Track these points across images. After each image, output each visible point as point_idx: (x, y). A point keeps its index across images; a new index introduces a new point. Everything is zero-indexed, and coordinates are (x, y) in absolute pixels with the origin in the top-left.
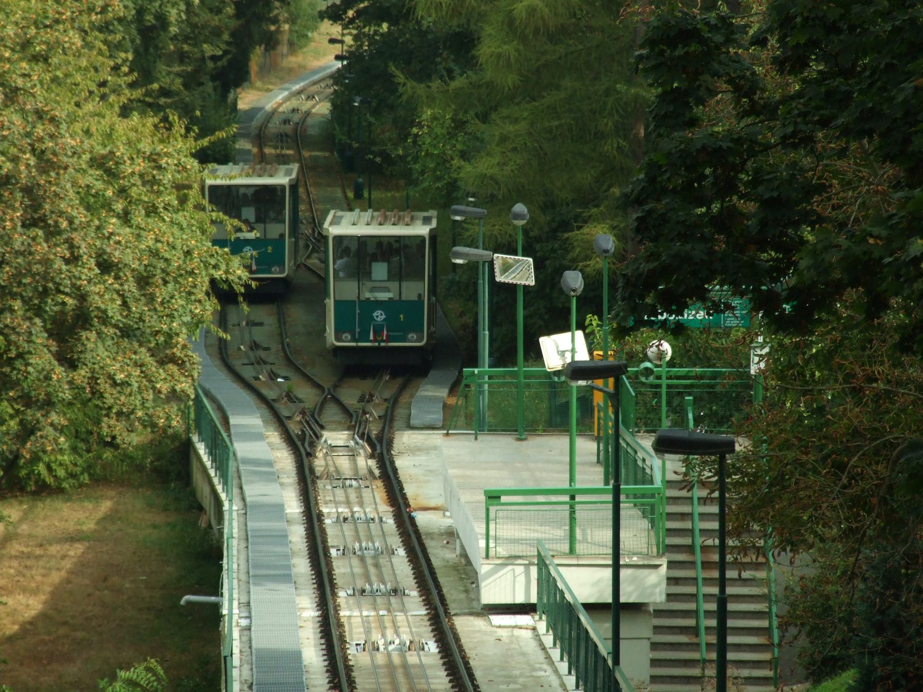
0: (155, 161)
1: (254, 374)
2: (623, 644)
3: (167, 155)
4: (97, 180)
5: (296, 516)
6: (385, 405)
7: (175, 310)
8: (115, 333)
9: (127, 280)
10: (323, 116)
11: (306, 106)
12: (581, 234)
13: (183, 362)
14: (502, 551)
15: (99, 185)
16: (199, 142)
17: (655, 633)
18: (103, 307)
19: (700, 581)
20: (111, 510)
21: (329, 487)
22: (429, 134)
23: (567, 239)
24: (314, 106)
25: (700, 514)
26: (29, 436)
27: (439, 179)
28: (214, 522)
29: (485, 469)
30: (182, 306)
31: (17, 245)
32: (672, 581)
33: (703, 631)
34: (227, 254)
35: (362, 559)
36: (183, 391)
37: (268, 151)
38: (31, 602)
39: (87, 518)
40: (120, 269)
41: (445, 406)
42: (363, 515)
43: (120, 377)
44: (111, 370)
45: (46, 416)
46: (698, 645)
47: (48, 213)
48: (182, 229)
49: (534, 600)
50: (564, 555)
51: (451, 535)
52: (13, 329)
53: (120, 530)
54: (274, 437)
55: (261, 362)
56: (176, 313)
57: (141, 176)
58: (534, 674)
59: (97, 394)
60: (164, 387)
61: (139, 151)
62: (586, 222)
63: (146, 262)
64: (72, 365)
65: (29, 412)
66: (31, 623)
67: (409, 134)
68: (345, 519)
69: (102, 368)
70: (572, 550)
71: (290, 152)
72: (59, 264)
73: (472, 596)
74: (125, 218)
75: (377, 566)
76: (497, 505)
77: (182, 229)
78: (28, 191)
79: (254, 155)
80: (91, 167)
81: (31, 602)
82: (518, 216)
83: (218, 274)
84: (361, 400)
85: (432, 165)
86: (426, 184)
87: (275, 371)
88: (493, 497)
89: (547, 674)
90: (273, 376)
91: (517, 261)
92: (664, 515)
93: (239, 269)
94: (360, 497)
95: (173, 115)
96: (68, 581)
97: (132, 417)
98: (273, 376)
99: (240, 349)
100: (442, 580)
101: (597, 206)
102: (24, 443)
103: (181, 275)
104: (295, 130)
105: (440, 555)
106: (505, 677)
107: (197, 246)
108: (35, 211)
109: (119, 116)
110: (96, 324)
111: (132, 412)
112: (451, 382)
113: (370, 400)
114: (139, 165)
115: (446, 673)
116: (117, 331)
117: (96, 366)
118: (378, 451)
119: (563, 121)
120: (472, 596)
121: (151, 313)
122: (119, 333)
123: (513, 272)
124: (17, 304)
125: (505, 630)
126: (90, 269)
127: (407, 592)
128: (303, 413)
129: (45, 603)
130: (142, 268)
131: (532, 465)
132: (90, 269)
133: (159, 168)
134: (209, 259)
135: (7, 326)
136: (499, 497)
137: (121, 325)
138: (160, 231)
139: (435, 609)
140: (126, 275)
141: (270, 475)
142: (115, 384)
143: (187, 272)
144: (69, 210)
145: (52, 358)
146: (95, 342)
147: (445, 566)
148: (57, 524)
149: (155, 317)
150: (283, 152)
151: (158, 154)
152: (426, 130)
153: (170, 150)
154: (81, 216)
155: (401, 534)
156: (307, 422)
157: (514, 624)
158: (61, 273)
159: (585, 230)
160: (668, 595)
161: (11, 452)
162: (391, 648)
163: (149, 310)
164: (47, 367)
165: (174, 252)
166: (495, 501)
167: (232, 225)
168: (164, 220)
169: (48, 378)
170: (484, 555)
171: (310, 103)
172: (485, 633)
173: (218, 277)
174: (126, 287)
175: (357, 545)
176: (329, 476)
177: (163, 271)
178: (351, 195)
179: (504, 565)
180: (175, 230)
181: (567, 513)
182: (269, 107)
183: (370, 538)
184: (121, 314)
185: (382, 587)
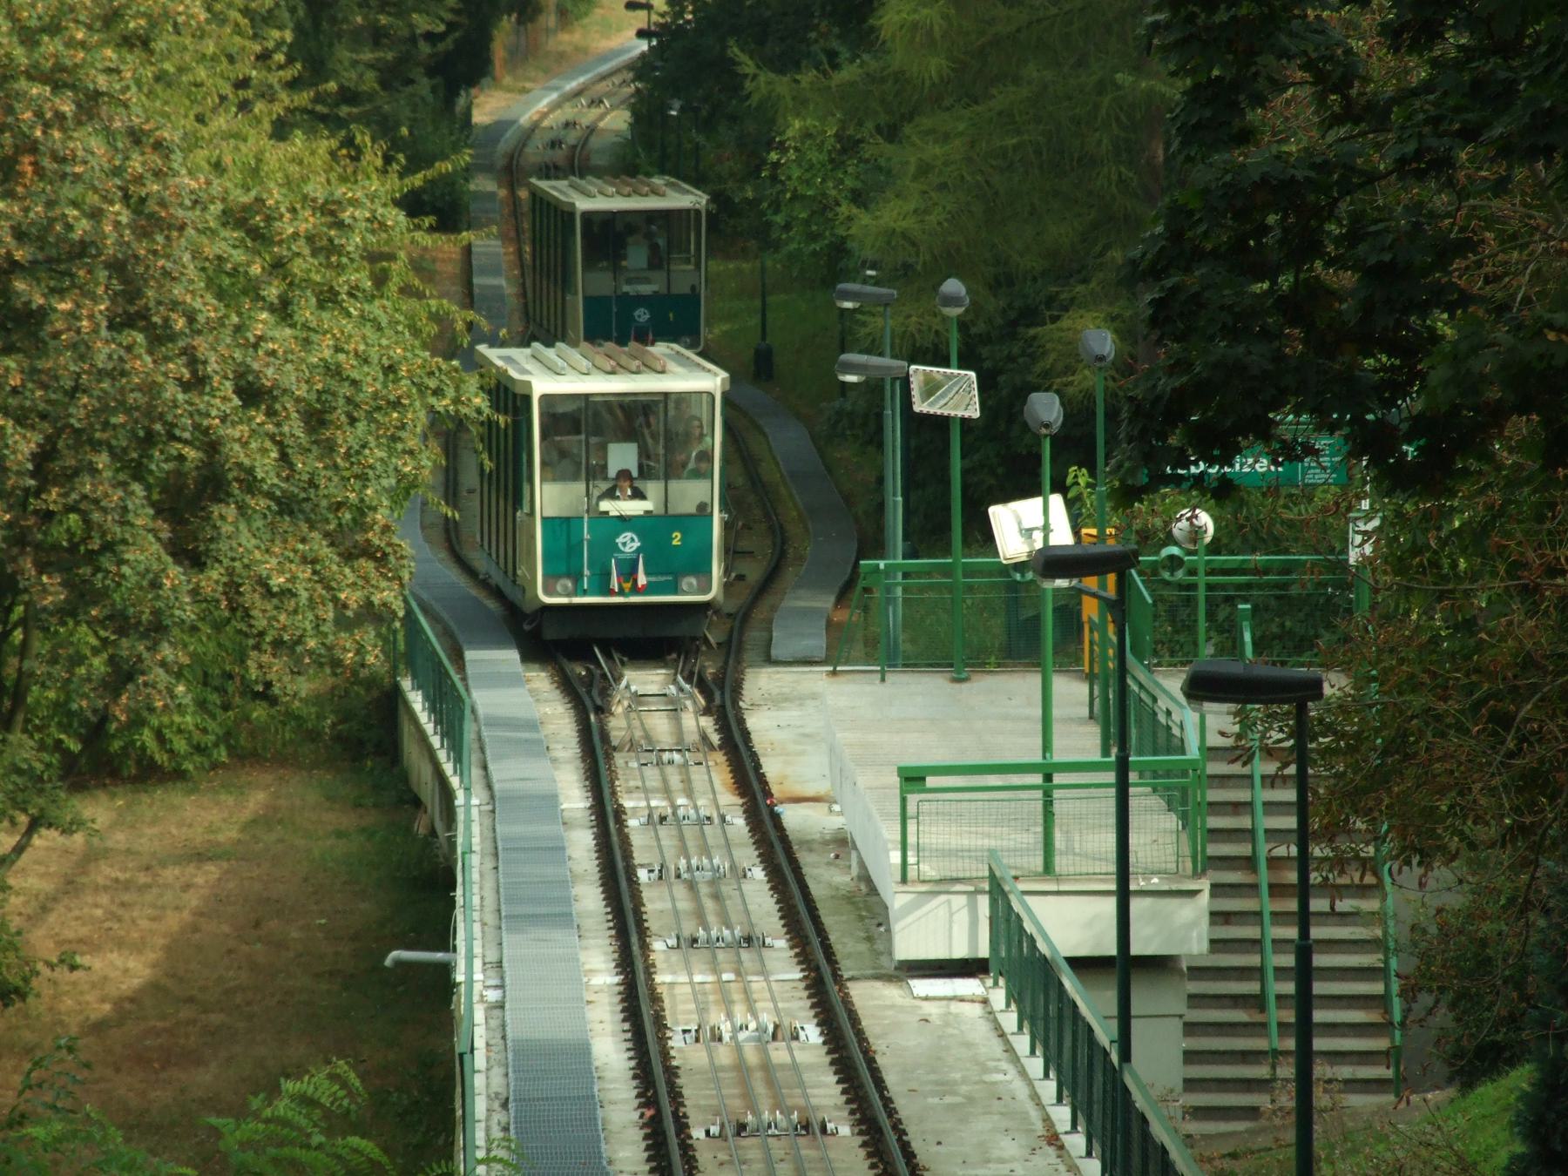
0: (332, 213)
2: (1136, 1026)
3: (354, 203)
4: (235, 247)
5: (579, 815)
7: (371, 467)
8: (269, 507)
9: (287, 417)
10: (618, 133)
13: (385, 555)
14: (929, 870)
16: (407, 181)
18: (247, 462)
19: (1267, 918)
22: (798, 162)
23: (1034, 338)
24: (602, 117)
27: (813, 237)
30: (382, 460)
31: (100, 360)
34: (456, 370)
35: (692, 886)
39: (224, 820)
40: (275, 399)
43: (278, 581)
44: (263, 570)
45: (153, 648)
46: (1264, 1025)
48: (379, 328)
49: (984, 951)
50: (1033, 876)
51: (842, 843)
57: (310, 239)
62: (1066, 309)
63: (319, 386)
65: (125, 642)
67: (764, 162)
69: (247, 567)
72: (171, 391)
73: (880, 946)
74: (283, 310)
75: (717, 897)
77: (379, 328)
78: (118, 267)
80: (224, 225)
82: (951, 301)
83: (441, 404)
85: (803, 215)
86: (793, 246)
88: (913, 779)
89: (1008, 1077)
91: (949, 377)
93: (476, 395)
95: (363, 133)
97: (299, 649)
100: (828, 920)
101: (1085, 281)
103: (379, 408)
105: (824, 878)
107: (405, 358)
108: (131, 301)
110: (236, 492)
111: (300, 641)
112: (837, 590)
114: (306, 220)
115: (835, 1078)
118: (718, 701)
121: (329, 473)
122: (275, 508)
123: (943, 396)
124: (102, 460)
126: (225, 399)
127: (768, 941)
130: (314, 396)
133: (340, 225)
135: (85, 497)
137: (278, 493)
139: (817, 969)
140: (285, 409)
142: (269, 593)
143: (388, 402)
144: (188, 299)
145: (162, 551)
148: (174, 831)
149: (336, 479)
152: (792, 155)
153: (359, 194)
154: (208, 308)
155: (759, 843)
157: (950, 993)
158: (176, 407)
159: (1065, 323)
161: (95, 711)
164: (155, 567)
165: (366, 369)
166: (916, 786)
168: (349, 315)
169: (155, 585)
171: (595, 112)
172: (902, 1009)
173: (441, 409)
174: (286, 429)
177: (349, 400)
180: (368, 331)
181: (1039, 805)
182: (525, 119)
183: (705, 850)
184: (278, 476)
185: (726, 933)
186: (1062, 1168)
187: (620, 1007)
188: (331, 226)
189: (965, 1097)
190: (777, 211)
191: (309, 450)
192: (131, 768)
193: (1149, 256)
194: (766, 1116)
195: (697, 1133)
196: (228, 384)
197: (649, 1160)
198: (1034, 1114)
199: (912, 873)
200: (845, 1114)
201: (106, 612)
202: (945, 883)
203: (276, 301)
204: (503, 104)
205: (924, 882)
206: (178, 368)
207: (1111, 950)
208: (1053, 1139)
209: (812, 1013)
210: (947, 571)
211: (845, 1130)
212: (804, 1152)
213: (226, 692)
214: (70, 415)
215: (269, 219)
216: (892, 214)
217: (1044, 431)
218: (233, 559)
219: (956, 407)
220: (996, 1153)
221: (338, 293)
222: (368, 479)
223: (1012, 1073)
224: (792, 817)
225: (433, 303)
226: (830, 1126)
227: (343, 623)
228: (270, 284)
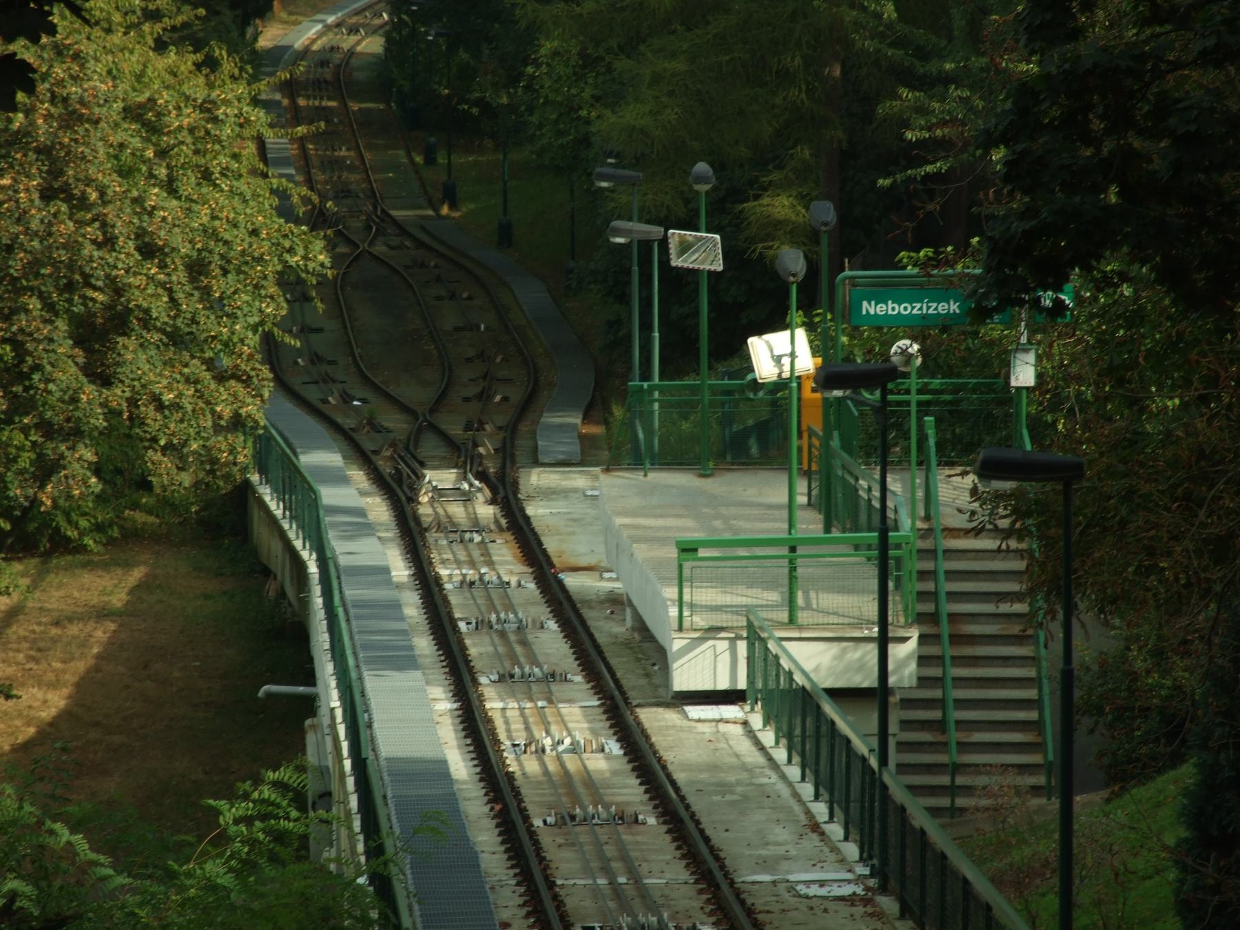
0: (208, 110)
1: (322, 397)
3: (227, 102)
4: (132, 136)
5: (405, 580)
6: (502, 435)
7: (238, 308)
8: (161, 340)
9: (175, 269)
10: (373, 55)
11: (347, 42)
12: (760, 205)
13: (249, 377)
14: (700, 621)
15: (136, 142)
16: (254, 86)
17: (902, 730)
18: (145, 305)
19: (948, 661)
20: (147, 575)
21: (445, 542)
22: (549, 74)
23: (741, 212)
24: (359, 43)
25: (947, 572)
26: (50, 476)
27: (560, 134)
28: (290, 591)
29: (661, 516)
30: (247, 302)
31: (35, 225)
32: (923, 660)
33: (952, 726)
34: (305, 233)
35: (503, 634)
36: (249, 416)
37: (302, 102)
38: (49, 696)
39: (115, 586)
40: (166, 255)
41: (582, 437)
42: (495, 578)
43: (168, 397)
44: (156, 389)
45: (72, 448)
46: (945, 744)
47: (71, 181)
48: (245, 201)
49: (742, 684)
50: (780, 625)
51: (616, 602)
52: (31, 334)
53: (160, 601)
54: (358, 476)
55: (328, 379)
56: (239, 313)
57: (191, 130)
58: (755, 781)
59: (136, 420)
60: (225, 410)
61: (187, 98)
62: (765, 189)
63: (199, 246)
64: (105, 381)
65: (51, 445)
66: (51, 724)
67: (521, 74)
68: (472, 583)
69: (143, 386)
70: (792, 621)
71: (333, 104)
72: (88, 249)
73: (656, 681)
74: (171, 187)
75: (524, 643)
76: (694, 560)
77: (245, 201)
78: (45, 152)
79: (285, 108)
80: (124, 119)
81: (49, 696)
82: (701, 179)
83: (293, 260)
84: (468, 427)
85: (554, 116)
86: (545, 141)
87: (349, 392)
88: (687, 549)
89: (772, 781)
90: (346, 398)
91: (701, 238)
92: (915, 575)
93: (321, 253)
94: (486, 553)
95: (221, 49)
96: (96, 669)
97: (185, 450)
98: (346, 398)
99: (296, 363)
100: (613, 662)
101: (780, 167)
102: (42, 487)
103: (247, 263)
104: (336, 74)
105: (607, 629)
106: (717, 785)
107: (265, 223)
108: (56, 178)
109: (154, 50)
110: (137, 328)
111: (185, 443)
112: (583, 409)
113: (481, 427)
114: (189, 116)
115: (638, 781)
116: (164, 337)
117: (136, 383)
118: (502, 494)
119: (736, 55)
120: (656, 681)
121: (207, 312)
122: (165, 340)
123: (693, 253)
124: (34, 304)
125: (707, 724)
126: (128, 254)
127: (569, 676)
128: (393, 445)
129: (70, 697)
130: (195, 254)
131: (724, 511)
132: (128, 254)
133: (215, 120)
134: (281, 240)
135: (21, 330)
136: (695, 550)
137: (168, 329)
138: (217, 204)
139: (612, 698)
140: (174, 262)
141: (361, 527)
142: (160, 407)
143: (253, 258)
144: (100, 176)
145: (79, 372)
146: (134, 351)
147: (614, 643)
148: (76, 594)
149: (213, 317)
150: (324, 104)
151: (213, 102)
152: (544, 69)
153: (229, 96)
154: (115, 185)
155: (549, 602)
156: (402, 458)
157: (717, 717)
158: (93, 261)
159: (766, 201)
160: (920, 679)
161: (26, 498)
162: (561, 748)
163: (204, 308)
164: (74, 385)
165: (236, 232)
166: (690, 555)
167: (299, 195)
168: (222, 191)
169: (74, 400)
170: (675, 625)
171: (353, 39)
172: (682, 729)
173: (294, 264)
174: (174, 278)
175: (493, 617)
176: (440, 527)
177: (222, 256)
178: (419, 159)
179: (702, 640)
180: (236, 201)
181: (786, 571)
182: (298, 45)
184: (169, 316)
185: (536, 670)
186: (826, 850)
187: (461, 727)
188: (208, 121)
189: (742, 796)
190: (531, 114)
191: (192, 295)
192: (45, 544)
193: (1001, 127)
194: (591, 809)
195: (537, 823)
196: (131, 243)
197: (503, 843)
198: (797, 808)
199: (686, 624)
200: (650, 808)
201: (35, 420)
202: (713, 631)
203: (165, 179)
204: (280, 32)
205: (695, 630)
206: (92, 231)
207: (868, 680)
208: (815, 827)
209: (612, 731)
210: (695, 390)
211: (652, 821)
212: (624, 837)
213: (115, 485)
214: (10, 267)
215: (159, 115)
216: (633, 114)
217: (792, 279)
218: (133, 380)
219: (703, 262)
220: (771, 838)
221: (213, 173)
222: (236, 318)
223: (774, 777)
224: (572, 581)
225: (275, 181)
226: (641, 817)
227: (217, 429)
228: (161, 165)
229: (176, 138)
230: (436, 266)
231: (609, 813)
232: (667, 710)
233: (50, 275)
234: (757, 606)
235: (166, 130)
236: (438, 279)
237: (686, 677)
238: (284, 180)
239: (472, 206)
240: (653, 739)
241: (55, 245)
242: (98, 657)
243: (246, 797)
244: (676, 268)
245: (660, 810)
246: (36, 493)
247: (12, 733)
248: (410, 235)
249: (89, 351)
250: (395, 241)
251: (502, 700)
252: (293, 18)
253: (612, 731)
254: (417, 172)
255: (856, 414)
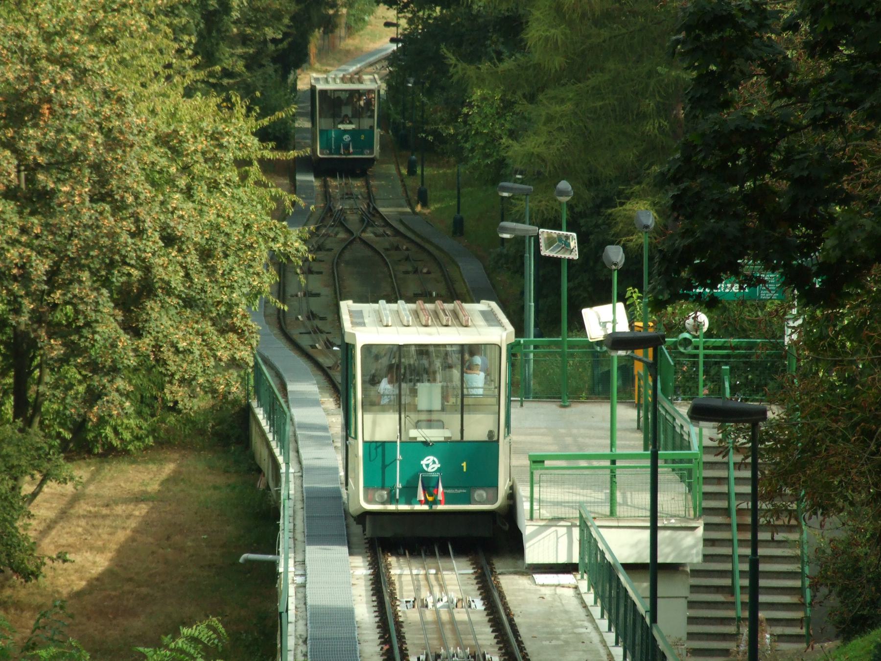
0: (217, 139)
1: (311, 343)
2: (660, 603)
4: (161, 157)
8: (178, 303)
9: (189, 253)
13: (243, 331)
14: (546, 513)
15: (164, 162)
18: (166, 278)
20: (174, 471)
22: (479, 114)
23: (610, 214)
26: (96, 401)
27: (487, 156)
28: (271, 484)
31: (85, 219)
32: (708, 542)
36: (242, 359)
39: (151, 479)
40: (183, 242)
43: (182, 345)
44: (174, 338)
45: (111, 381)
46: (733, 603)
47: (114, 188)
48: (243, 204)
49: (576, 559)
50: (604, 517)
52: (82, 299)
55: (318, 331)
56: (236, 284)
57: (204, 153)
60: (224, 355)
62: (628, 199)
63: (207, 236)
64: (137, 333)
65: (96, 378)
66: (97, 579)
67: (460, 113)
69: (165, 336)
70: (612, 513)
72: (125, 237)
74: (188, 193)
76: (541, 469)
78: (96, 167)
80: (156, 145)
81: (98, 559)
82: (563, 193)
83: (276, 246)
85: (481, 144)
87: (331, 340)
88: (538, 461)
89: (588, 630)
92: (701, 480)
93: (296, 241)
95: (236, 96)
96: (133, 539)
97: (194, 383)
101: (639, 183)
102: (91, 407)
103: (241, 249)
106: (549, 633)
107: (256, 220)
108: (103, 187)
110: (160, 294)
111: (194, 379)
115: (491, 629)
116: (180, 301)
117: (160, 335)
121: (212, 285)
122: (181, 303)
124: (85, 276)
125: (548, 588)
126: (154, 242)
130: (204, 242)
132: (154, 242)
133: (221, 146)
134: (268, 232)
135: (75, 296)
137: (184, 296)
138: (221, 206)
140: (188, 248)
142: (177, 351)
143: (246, 246)
144: (135, 185)
148: (122, 484)
152: (475, 110)
154: (146, 191)
157: (556, 583)
158: (127, 246)
159: (628, 206)
161: (79, 415)
162: (439, 605)
166: (539, 466)
168: (225, 195)
169: (113, 346)
174: (189, 259)
177: (224, 244)
178: (404, 171)
179: (547, 527)
180: (236, 205)
181: (608, 477)
184: (184, 286)
189: (564, 641)
190: (466, 142)
196: (157, 234)
198: (603, 652)
199: (536, 515)
200: (496, 649)
205: (542, 520)
214: (68, 250)
217: (614, 267)
225: (273, 190)
229: (192, 159)
230: (407, 249)
231: (465, 653)
232: (521, 577)
233: (97, 256)
234: (587, 502)
235: (185, 153)
236: (407, 259)
237: (534, 553)
238: (280, 189)
239: (437, 206)
240: (508, 599)
241: (100, 235)
242: (135, 531)
243: (166, 647)
244: (545, 257)
245: (503, 651)
246: (85, 412)
247: (69, 585)
248: (391, 226)
249: (127, 310)
250: (381, 230)
251: (401, 568)
252: (324, 68)
253: (479, 592)
254: (402, 181)
255: (672, 363)
